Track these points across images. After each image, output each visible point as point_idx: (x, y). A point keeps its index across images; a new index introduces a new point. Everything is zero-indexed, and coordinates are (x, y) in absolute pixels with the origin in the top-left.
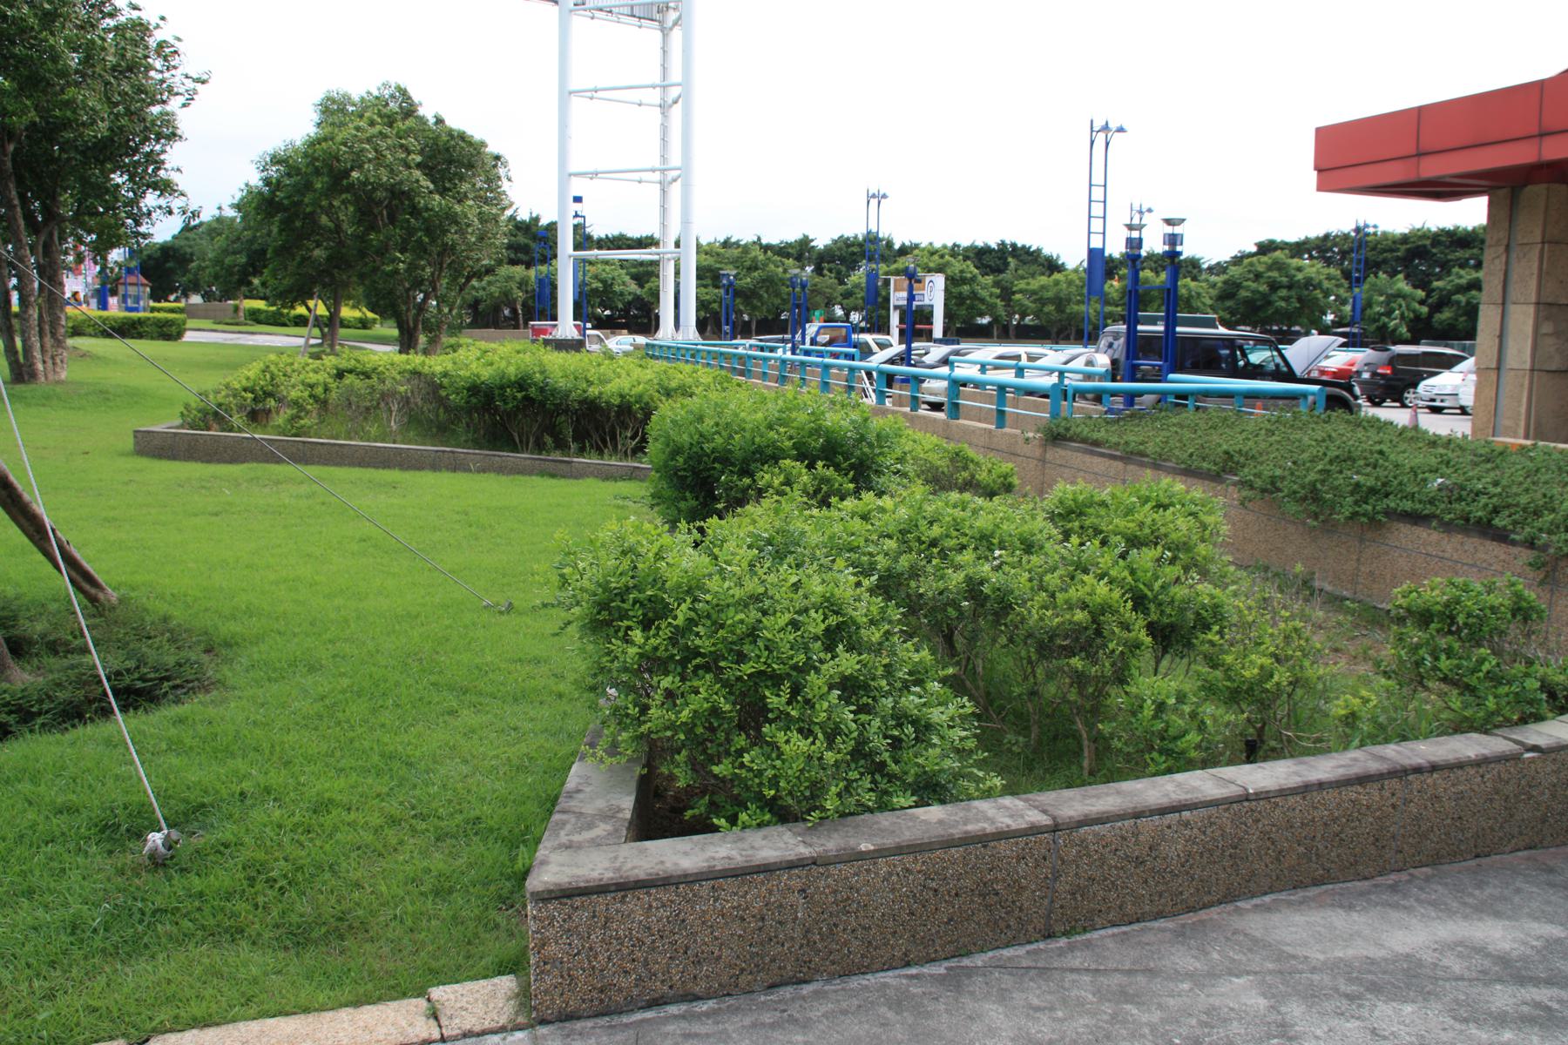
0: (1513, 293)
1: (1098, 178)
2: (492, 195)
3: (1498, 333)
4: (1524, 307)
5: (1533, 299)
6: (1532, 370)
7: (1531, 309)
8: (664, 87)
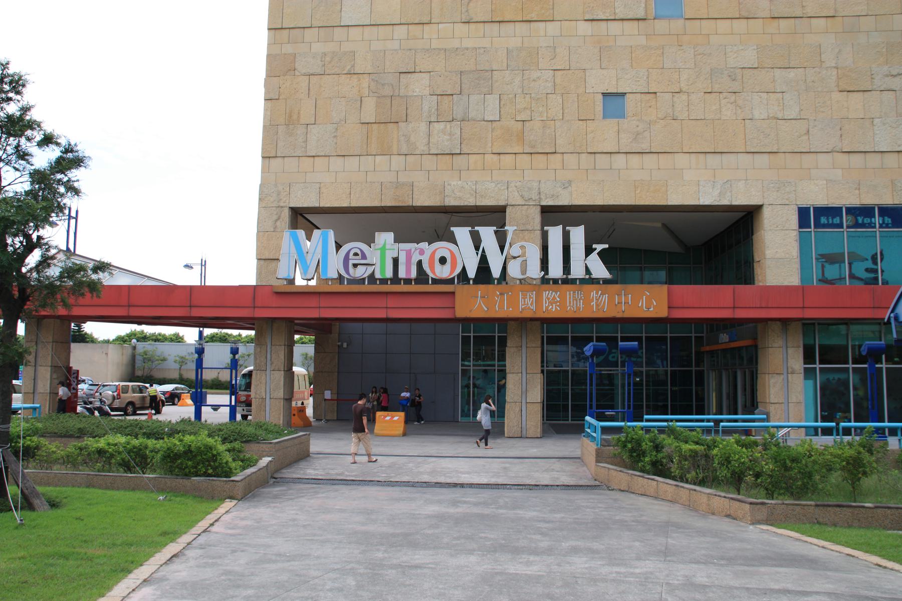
0: (40, 361)
1: (203, 267)
2: (226, 424)
3: (33, 378)
4: (46, 367)
5: (50, 365)
6: (50, 393)
7: (49, 369)
8: (190, 306)
